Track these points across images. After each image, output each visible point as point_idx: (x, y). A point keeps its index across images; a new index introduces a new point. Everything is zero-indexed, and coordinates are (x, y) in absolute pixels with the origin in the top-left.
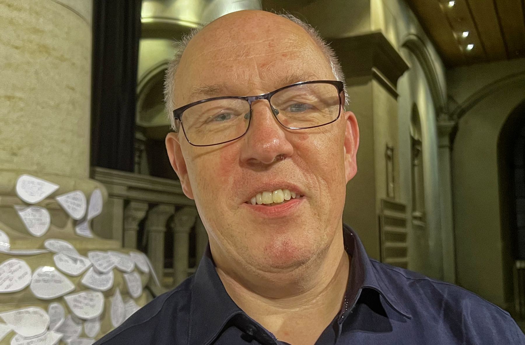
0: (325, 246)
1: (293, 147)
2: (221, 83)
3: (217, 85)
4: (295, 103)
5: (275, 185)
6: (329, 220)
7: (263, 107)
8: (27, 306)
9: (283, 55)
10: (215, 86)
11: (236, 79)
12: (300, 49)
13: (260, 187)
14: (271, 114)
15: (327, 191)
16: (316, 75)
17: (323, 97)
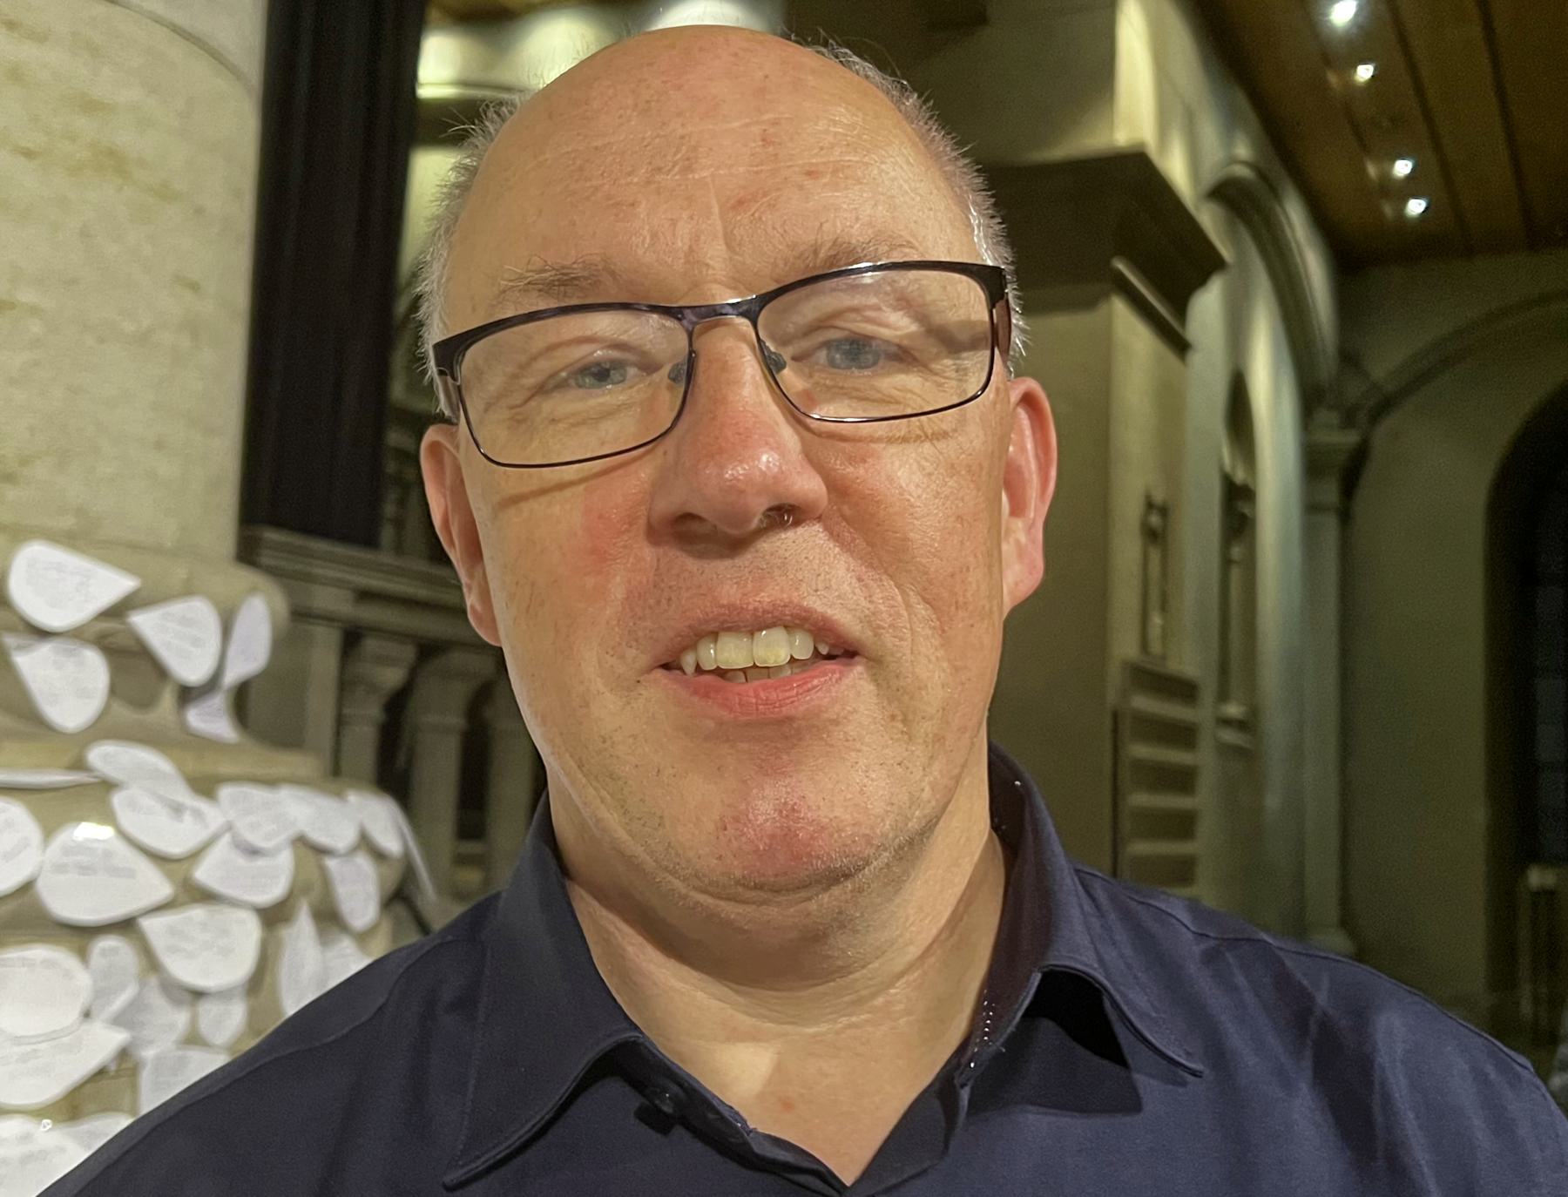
0: (924, 825)
1: (827, 487)
2: (595, 257)
3: (584, 262)
4: (845, 333)
5: (760, 614)
6: (939, 739)
7: (730, 342)
8: (25, 942)
9: (809, 174)
10: (574, 269)
11: (646, 246)
12: (867, 158)
13: (711, 615)
14: (756, 366)
15: (936, 642)
16: (917, 244)
17: (937, 320)
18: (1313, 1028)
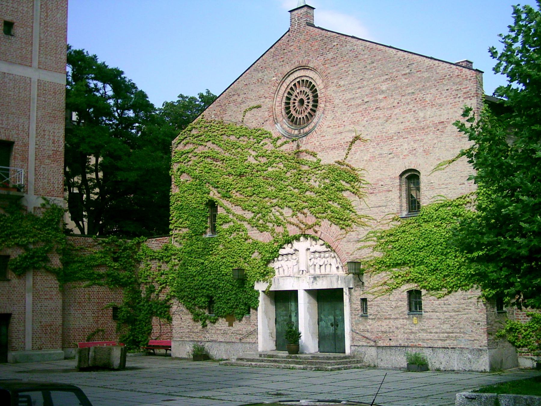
18: (314, 89)
